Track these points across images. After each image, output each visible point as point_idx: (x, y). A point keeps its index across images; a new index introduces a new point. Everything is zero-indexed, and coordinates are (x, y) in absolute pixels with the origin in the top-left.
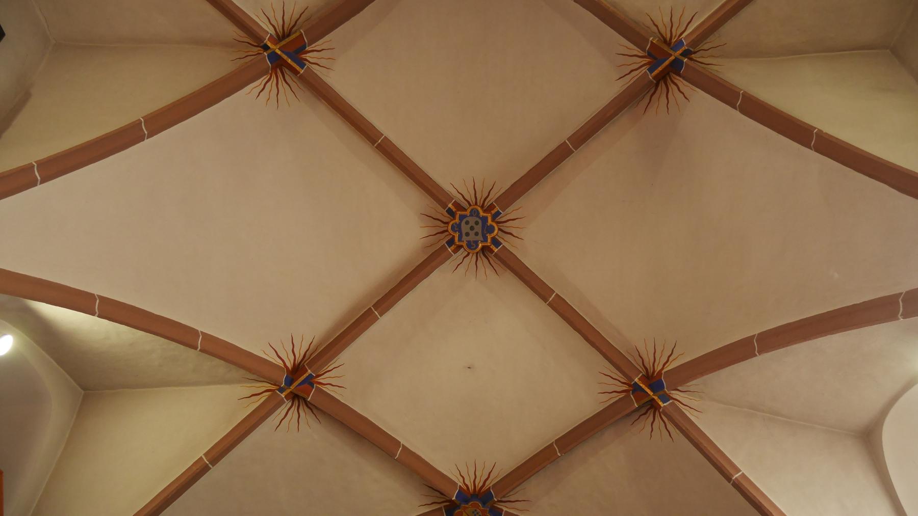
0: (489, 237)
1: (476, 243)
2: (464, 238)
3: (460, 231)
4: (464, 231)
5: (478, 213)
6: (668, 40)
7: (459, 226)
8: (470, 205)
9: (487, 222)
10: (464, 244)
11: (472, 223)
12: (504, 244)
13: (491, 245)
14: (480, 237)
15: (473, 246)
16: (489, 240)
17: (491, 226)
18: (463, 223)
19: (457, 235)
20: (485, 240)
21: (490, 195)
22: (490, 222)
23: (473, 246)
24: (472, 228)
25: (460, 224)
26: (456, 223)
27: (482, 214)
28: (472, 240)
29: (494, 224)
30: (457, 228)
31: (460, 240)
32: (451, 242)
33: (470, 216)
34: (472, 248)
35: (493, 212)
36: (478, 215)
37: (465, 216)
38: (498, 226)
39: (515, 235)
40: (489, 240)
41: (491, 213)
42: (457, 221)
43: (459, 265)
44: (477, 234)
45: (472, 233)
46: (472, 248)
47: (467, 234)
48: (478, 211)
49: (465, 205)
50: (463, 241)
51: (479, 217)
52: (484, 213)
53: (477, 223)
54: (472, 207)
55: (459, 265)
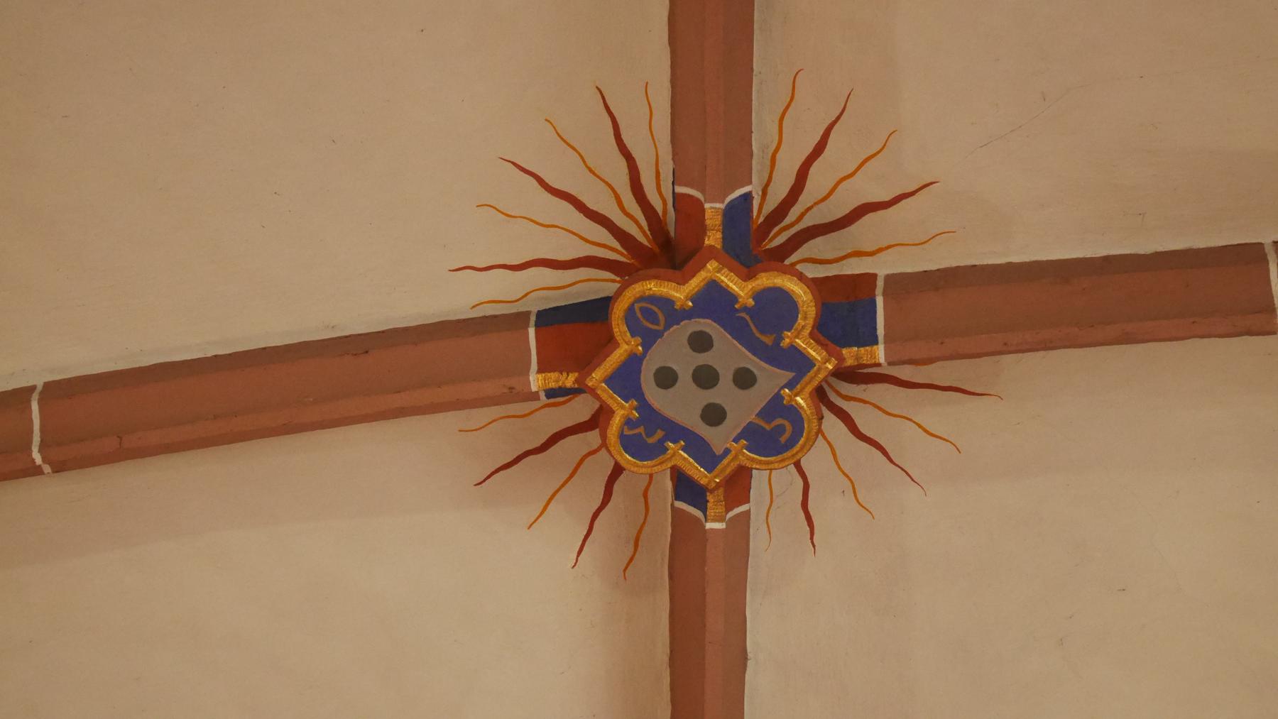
0: (801, 339)
1: (776, 407)
2: (717, 437)
3: (676, 432)
4: (690, 418)
5: (666, 302)
6: (820, 435)
7: (650, 417)
8: (618, 470)
9: (733, 298)
10: (746, 456)
11: (684, 362)
12: (882, 267)
13: (841, 359)
14: (770, 379)
15: (781, 429)
16: (814, 353)
17: (759, 296)
18: (656, 397)
19: (679, 455)
20: (798, 364)
21: (636, 154)
22: (741, 289)
23: (781, 429)
24: (706, 378)
25: (644, 406)
26: (628, 422)
27: (680, 293)
28: (752, 417)
29: (766, 280)
30: (649, 435)
31: (708, 458)
32: (686, 488)
33: (647, 346)
34: (783, 439)
35: (713, 239)
36: (674, 314)
37: (633, 364)
38: (792, 271)
39: (886, 197)
40: (814, 353)
41: (712, 253)
42: (622, 410)
43: (805, 504)
44: (744, 379)
45: (724, 394)
46: (783, 439)
47: (714, 415)
48: (654, 299)
49: (596, 284)
50: (727, 451)
51: (688, 314)
52: (683, 281)
53: (701, 342)
54: (626, 459)
55: (805, 504)
